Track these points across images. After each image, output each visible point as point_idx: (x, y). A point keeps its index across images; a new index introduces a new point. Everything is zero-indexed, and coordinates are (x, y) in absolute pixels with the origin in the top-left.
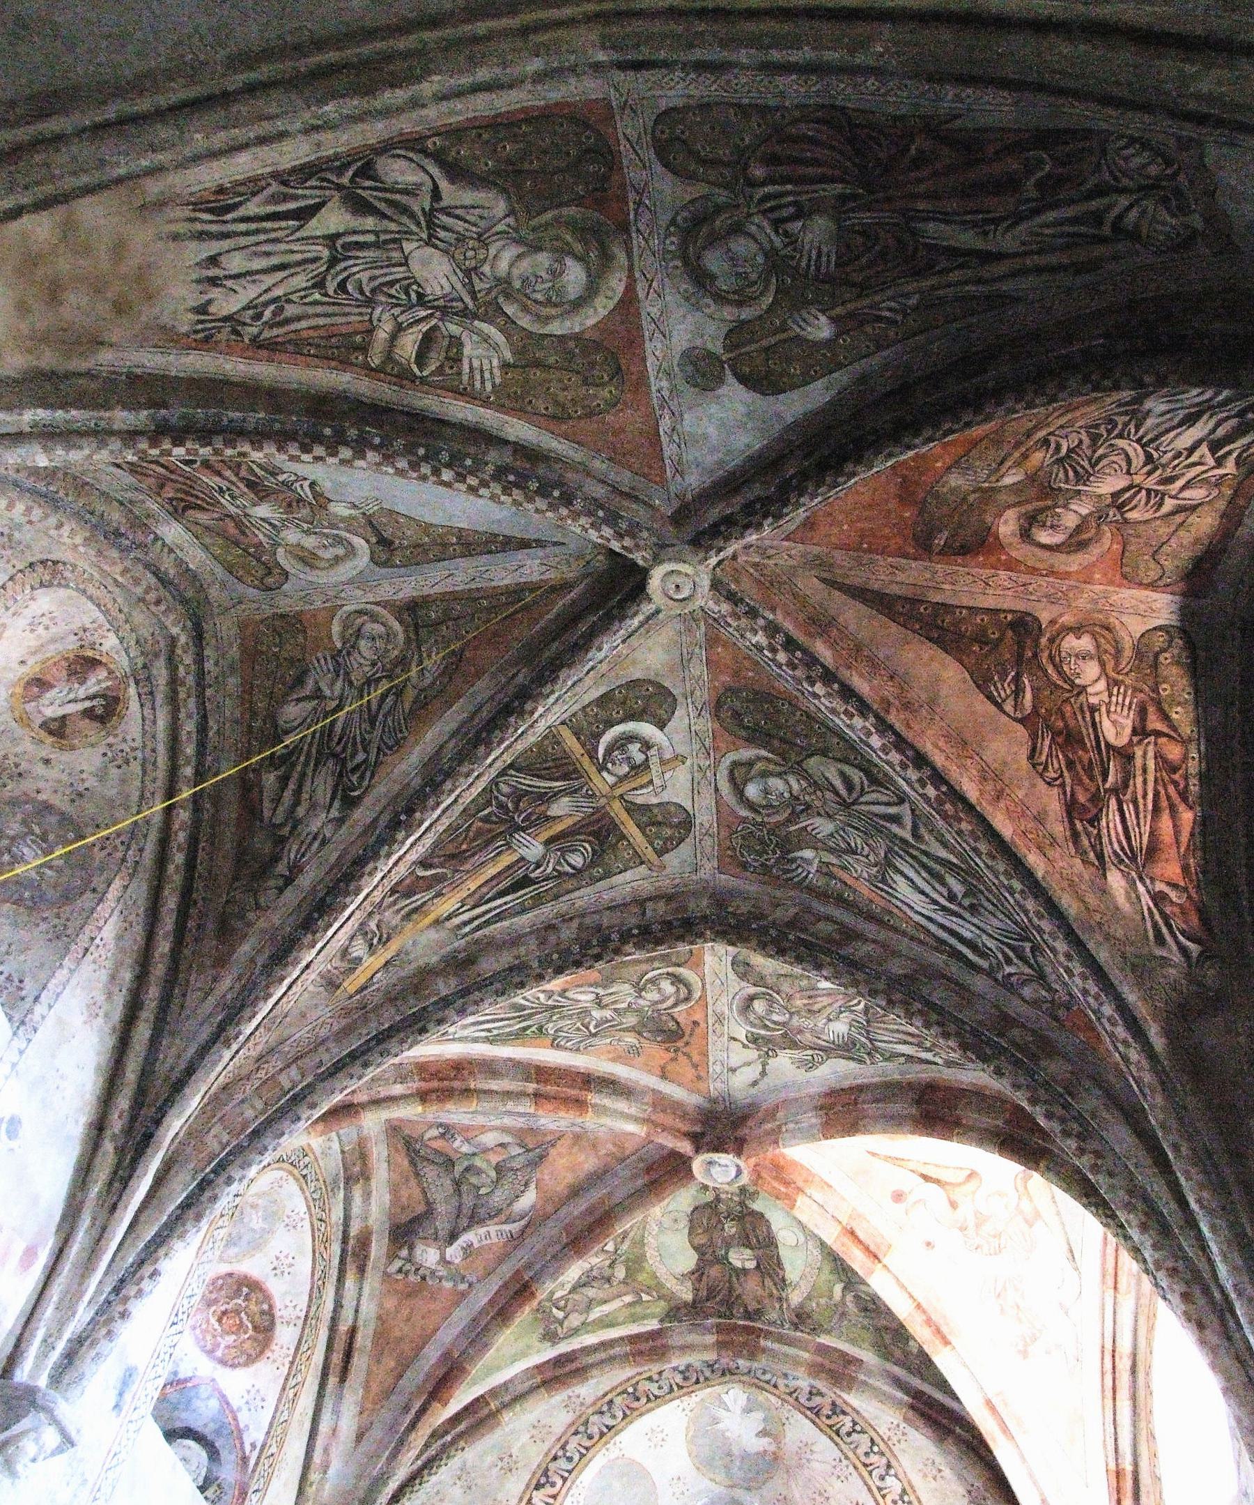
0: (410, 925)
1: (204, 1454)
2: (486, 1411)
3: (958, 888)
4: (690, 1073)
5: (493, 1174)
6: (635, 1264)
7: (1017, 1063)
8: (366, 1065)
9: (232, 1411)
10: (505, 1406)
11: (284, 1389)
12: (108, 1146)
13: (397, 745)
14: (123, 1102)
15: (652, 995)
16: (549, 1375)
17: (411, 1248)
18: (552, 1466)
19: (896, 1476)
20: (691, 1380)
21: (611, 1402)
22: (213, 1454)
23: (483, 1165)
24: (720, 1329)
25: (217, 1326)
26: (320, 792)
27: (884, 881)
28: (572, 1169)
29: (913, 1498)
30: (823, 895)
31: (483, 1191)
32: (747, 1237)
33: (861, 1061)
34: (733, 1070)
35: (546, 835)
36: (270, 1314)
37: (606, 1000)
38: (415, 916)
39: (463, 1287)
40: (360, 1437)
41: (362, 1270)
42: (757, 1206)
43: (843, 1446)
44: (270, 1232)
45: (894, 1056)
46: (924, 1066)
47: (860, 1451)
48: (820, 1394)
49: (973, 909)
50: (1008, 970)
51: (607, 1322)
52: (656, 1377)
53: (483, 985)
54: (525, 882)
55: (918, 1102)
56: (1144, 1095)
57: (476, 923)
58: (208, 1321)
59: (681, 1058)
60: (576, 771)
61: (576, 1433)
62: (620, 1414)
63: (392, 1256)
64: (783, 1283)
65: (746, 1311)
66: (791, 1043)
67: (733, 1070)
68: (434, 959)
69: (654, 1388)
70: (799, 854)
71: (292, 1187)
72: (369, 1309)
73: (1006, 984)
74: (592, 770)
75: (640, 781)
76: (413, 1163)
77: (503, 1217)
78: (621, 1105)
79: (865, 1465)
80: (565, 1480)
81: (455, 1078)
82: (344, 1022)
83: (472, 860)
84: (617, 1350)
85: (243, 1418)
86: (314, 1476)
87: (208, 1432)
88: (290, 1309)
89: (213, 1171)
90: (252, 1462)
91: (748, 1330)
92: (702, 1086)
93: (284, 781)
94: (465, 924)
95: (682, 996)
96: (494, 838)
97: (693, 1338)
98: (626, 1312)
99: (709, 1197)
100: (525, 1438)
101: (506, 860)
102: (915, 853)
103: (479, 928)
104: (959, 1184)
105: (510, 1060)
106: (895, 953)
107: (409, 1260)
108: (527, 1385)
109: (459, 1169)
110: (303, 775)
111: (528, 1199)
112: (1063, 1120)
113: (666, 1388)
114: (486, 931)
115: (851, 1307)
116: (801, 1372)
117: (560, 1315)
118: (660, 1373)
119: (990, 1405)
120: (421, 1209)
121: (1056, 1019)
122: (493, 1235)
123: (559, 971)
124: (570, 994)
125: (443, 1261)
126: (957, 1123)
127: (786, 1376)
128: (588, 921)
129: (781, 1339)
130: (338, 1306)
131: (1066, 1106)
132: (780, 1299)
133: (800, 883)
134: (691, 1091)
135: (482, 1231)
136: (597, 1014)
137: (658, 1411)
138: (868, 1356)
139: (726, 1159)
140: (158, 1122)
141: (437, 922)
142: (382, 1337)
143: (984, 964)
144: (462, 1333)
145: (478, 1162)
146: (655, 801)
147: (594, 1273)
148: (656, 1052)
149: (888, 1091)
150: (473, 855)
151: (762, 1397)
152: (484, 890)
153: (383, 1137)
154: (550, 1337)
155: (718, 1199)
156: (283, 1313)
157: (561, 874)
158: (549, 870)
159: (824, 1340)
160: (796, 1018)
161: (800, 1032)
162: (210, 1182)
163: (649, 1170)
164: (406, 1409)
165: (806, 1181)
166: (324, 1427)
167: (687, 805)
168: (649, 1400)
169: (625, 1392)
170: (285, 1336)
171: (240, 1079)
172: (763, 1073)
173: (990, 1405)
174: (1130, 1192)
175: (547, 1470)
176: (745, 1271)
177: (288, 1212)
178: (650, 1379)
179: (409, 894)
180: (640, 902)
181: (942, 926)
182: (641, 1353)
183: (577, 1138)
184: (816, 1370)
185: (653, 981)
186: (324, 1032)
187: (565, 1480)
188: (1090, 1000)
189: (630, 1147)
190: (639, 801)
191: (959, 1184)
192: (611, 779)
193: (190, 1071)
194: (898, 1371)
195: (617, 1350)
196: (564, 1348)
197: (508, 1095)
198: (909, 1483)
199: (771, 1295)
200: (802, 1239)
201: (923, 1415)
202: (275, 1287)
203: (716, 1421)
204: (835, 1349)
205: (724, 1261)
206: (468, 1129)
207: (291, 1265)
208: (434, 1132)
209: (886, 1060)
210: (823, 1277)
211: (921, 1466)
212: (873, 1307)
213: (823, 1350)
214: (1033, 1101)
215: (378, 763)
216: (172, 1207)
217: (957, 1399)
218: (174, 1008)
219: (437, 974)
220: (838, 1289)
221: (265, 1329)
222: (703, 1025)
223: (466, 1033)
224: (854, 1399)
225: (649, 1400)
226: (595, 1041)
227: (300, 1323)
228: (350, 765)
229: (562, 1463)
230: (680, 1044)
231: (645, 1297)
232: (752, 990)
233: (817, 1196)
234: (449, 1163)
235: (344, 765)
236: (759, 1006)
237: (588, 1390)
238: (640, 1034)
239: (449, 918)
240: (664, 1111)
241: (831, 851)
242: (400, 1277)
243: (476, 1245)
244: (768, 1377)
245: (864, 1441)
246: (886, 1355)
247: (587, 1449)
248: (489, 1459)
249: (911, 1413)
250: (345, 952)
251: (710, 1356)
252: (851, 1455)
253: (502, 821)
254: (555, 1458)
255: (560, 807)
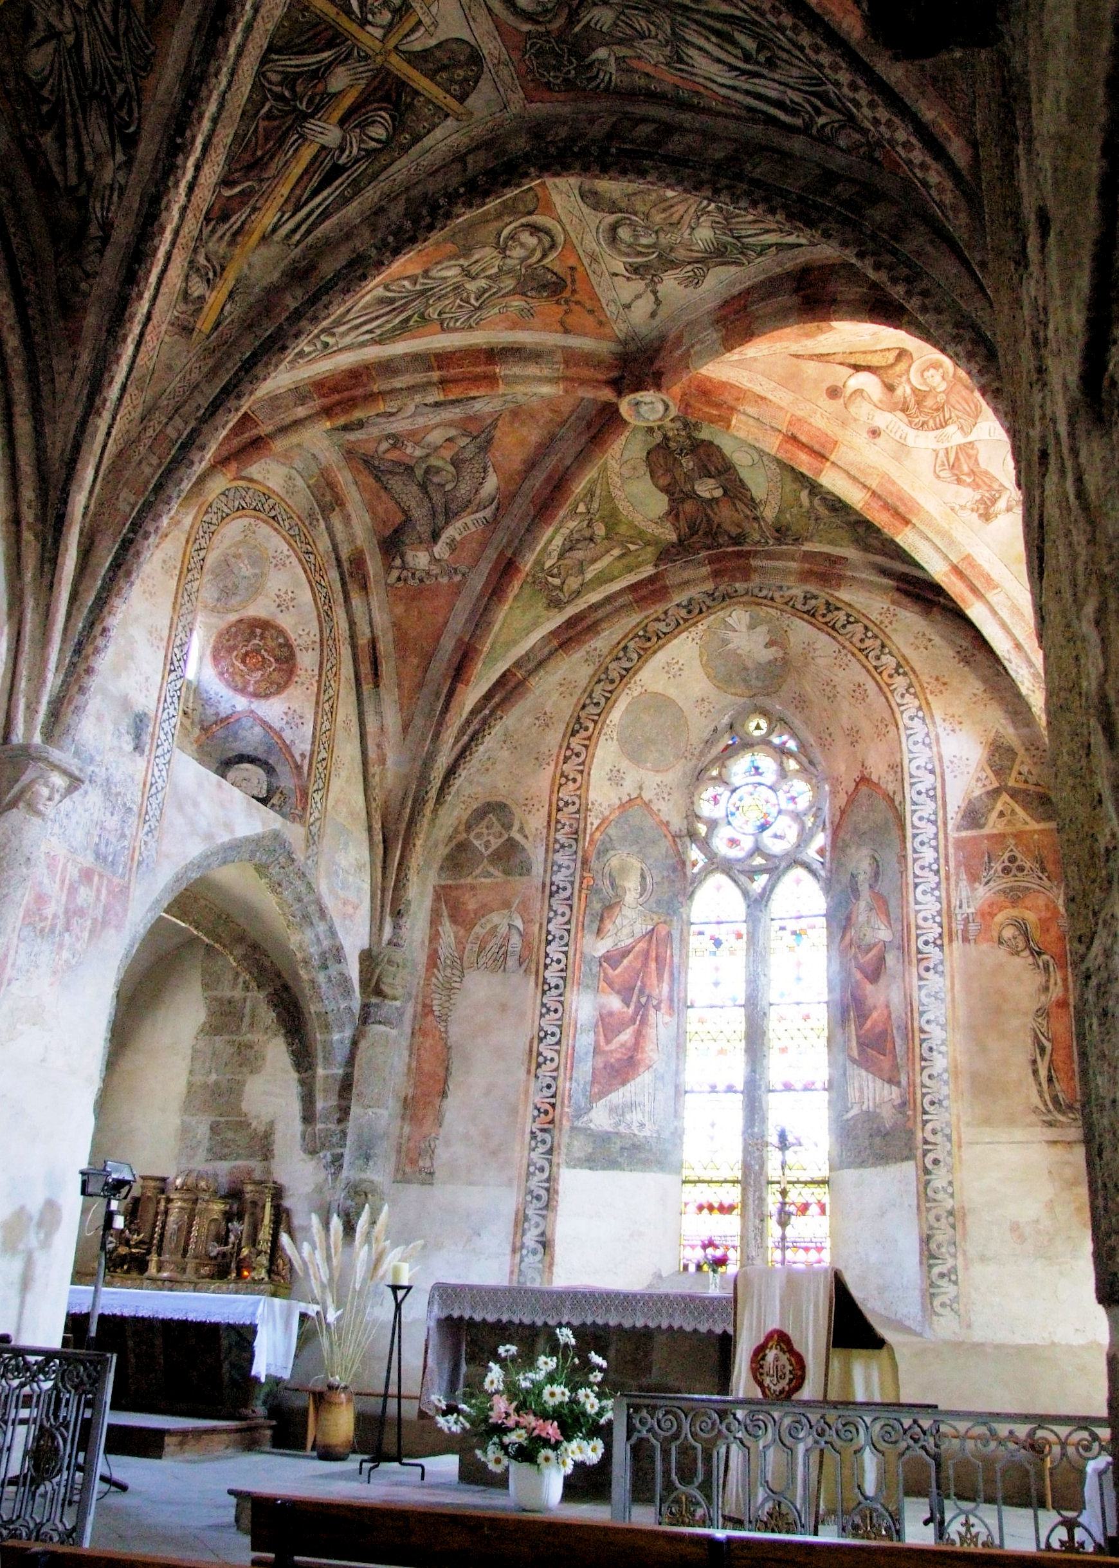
0: (237, 251)
1: (261, 772)
2: (512, 684)
3: (750, 45)
4: (590, 321)
5: (451, 468)
6: (612, 519)
7: (845, 221)
8: (239, 397)
9: (276, 733)
10: (531, 673)
11: (317, 703)
12: (28, 536)
13: (146, 64)
14: (28, 493)
15: (517, 252)
16: (565, 637)
17: (402, 557)
18: (583, 714)
19: (890, 653)
20: (694, 612)
21: (625, 648)
22: (270, 770)
23: (440, 463)
24: (711, 561)
25: (242, 667)
26: (98, 138)
27: (680, 60)
28: (522, 443)
29: (907, 669)
30: (631, 94)
31: (448, 487)
32: (705, 466)
33: (737, 263)
34: (628, 306)
35: (337, 114)
36: (288, 645)
37: (475, 269)
38: (240, 239)
39: (457, 578)
40: (406, 727)
41: (364, 587)
42: (704, 435)
43: (840, 638)
44: (263, 574)
45: (763, 249)
46: (796, 251)
47: (855, 640)
48: (815, 597)
49: (771, 63)
50: (821, 121)
51: (602, 579)
52: (662, 617)
53: (327, 288)
54: (337, 171)
55: (796, 291)
56: (947, 217)
57: (304, 228)
58: (233, 665)
59: (576, 308)
60: (338, 34)
61: (599, 681)
62: (635, 657)
63: (389, 568)
64: (753, 503)
65: (730, 537)
66: (668, 263)
67: (628, 306)
68: (276, 276)
69: (662, 627)
70: (594, 56)
71: (265, 530)
72: (381, 619)
73: (824, 139)
74: (353, 28)
75: (407, 27)
76: (378, 479)
77: (473, 507)
78: (532, 370)
79: (861, 650)
80: (595, 722)
81: (355, 386)
82: (211, 362)
83: (273, 165)
84: (621, 601)
85: (288, 735)
86: (374, 769)
87: (260, 753)
88: (305, 637)
89: (129, 531)
90: (306, 768)
91: (739, 555)
92: (607, 330)
93: (60, 139)
94: (294, 231)
95: (547, 245)
96: (285, 135)
97: (688, 574)
98: (619, 565)
99: (658, 438)
100: (555, 696)
101: (307, 153)
102: (697, 17)
103: (309, 232)
104: (892, 366)
105: (406, 354)
106: (715, 138)
107: (404, 567)
108: (546, 651)
109: (419, 472)
110: (76, 126)
111: (491, 483)
112: (891, 268)
113: (673, 624)
114: (318, 233)
115: (822, 511)
116: (792, 580)
117: (557, 581)
118: (666, 613)
119: (956, 570)
120: (399, 518)
121: (874, 161)
122: (470, 524)
123: (396, 252)
124: (433, 273)
125: (434, 560)
126: (834, 301)
127: (781, 588)
128: (415, 192)
129: (770, 556)
130: (352, 624)
131: (894, 252)
132: (756, 519)
133: (607, 89)
134: (599, 337)
135: (459, 524)
136: (472, 286)
137: (670, 645)
138: (851, 553)
139: (647, 396)
140: (64, 502)
141: (264, 239)
142: (402, 641)
143: (799, 122)
144: (467, 621)
145: (434, 461)
146: (433, 42)
147: (576, 536)
148: (549, 308)
149: (769, 287)
150: (272, 158)
151: (763, 612)
152: (298, 192)
153: (342, 464)
154: (555, 604)
155: (666, 438)
156: (299, 641)
157: (370, 153)
158: (355, 151)
159: (807, 547)
160: (662, 235)
161: (672, 249)
162: (131, 541)
163: (589, 425)
164: (437, 695)
165: (738, 399)
166: (372, 726)
167: (465, 35)
168: (659, 638)
169: (636, 636)
170: (307, 660)
171: (131, 443)
172: (658, 302)
173: (956, 570)
174: (957, 325)
175: (579, 718)
176: (714, 500)
177: (271, 553)
178: (658, 620)
179: (224, 217)
180: (460, 158)
181: (748, 93)
182: (643, 599)
183: (515, 414)
184: (805, 576)
185: (512, 237)
186: (195, 376)
187: (595, 722)
188: (883, 129)
189: (566, 409)
190: (417, 47)
191: (892, 366)
192: (378, 33)
193: (77, 447)
194: (879, 559)
195: (621, 601)
196: (570, 611)
197: (412, 389)
198: (903, 656)
199: (747, 517)
200: (756, 457)
201: (907, 594)
202: (285, 621)
203: (725, 642)
204: (821, 553)
205: (692, 495)
206: (412, 433)
207: (293, 599)
208: (385, 445)
209: (760, 255)
210: (787, 489)
211: (912, 640)
212: (838, 506)
213: (808, 556)
214: (861, 255)
215: (139, 90)
216: (103, 572)
217: (923, 568)
218: (46, 390)
219: (284, 289)
220: (804, 495)
221: (286, 659)
222: (580, 269)
223: (348, 340)
224: (844, 595)
225: (659, 638)
226: (484, 313)
227: (317, 646)
228: (115, 100)
229: (592, 710)
230: (566, 294)
231: (632, 547)
232: (612, 218)
233: (751, 410)
234: (409, 469)
235: (107, 99)
236: (624, 233)
237: (603, 642)
238: (524, 294)
239: (274, 230)
240: (576, 365)
241: (621, 42)
242: (401, 584)
243: (458, 538)
244: (764, 593)
245: (859, 628)
246: (867, 548)
247: (611, 692)
248: (528, 720)
249: (897, 595)
250: (185, 295)
251: (709, 586)
252: (847, 644)
253: (287, 113)
254: (584, 707)
255: (339, 80)
